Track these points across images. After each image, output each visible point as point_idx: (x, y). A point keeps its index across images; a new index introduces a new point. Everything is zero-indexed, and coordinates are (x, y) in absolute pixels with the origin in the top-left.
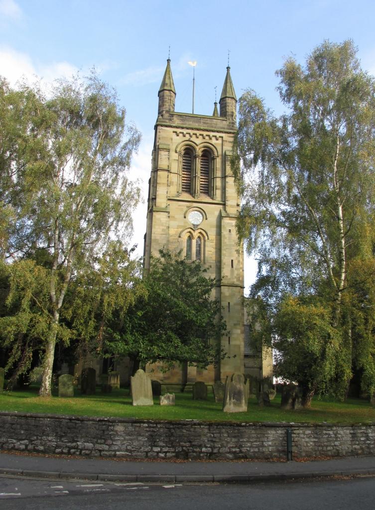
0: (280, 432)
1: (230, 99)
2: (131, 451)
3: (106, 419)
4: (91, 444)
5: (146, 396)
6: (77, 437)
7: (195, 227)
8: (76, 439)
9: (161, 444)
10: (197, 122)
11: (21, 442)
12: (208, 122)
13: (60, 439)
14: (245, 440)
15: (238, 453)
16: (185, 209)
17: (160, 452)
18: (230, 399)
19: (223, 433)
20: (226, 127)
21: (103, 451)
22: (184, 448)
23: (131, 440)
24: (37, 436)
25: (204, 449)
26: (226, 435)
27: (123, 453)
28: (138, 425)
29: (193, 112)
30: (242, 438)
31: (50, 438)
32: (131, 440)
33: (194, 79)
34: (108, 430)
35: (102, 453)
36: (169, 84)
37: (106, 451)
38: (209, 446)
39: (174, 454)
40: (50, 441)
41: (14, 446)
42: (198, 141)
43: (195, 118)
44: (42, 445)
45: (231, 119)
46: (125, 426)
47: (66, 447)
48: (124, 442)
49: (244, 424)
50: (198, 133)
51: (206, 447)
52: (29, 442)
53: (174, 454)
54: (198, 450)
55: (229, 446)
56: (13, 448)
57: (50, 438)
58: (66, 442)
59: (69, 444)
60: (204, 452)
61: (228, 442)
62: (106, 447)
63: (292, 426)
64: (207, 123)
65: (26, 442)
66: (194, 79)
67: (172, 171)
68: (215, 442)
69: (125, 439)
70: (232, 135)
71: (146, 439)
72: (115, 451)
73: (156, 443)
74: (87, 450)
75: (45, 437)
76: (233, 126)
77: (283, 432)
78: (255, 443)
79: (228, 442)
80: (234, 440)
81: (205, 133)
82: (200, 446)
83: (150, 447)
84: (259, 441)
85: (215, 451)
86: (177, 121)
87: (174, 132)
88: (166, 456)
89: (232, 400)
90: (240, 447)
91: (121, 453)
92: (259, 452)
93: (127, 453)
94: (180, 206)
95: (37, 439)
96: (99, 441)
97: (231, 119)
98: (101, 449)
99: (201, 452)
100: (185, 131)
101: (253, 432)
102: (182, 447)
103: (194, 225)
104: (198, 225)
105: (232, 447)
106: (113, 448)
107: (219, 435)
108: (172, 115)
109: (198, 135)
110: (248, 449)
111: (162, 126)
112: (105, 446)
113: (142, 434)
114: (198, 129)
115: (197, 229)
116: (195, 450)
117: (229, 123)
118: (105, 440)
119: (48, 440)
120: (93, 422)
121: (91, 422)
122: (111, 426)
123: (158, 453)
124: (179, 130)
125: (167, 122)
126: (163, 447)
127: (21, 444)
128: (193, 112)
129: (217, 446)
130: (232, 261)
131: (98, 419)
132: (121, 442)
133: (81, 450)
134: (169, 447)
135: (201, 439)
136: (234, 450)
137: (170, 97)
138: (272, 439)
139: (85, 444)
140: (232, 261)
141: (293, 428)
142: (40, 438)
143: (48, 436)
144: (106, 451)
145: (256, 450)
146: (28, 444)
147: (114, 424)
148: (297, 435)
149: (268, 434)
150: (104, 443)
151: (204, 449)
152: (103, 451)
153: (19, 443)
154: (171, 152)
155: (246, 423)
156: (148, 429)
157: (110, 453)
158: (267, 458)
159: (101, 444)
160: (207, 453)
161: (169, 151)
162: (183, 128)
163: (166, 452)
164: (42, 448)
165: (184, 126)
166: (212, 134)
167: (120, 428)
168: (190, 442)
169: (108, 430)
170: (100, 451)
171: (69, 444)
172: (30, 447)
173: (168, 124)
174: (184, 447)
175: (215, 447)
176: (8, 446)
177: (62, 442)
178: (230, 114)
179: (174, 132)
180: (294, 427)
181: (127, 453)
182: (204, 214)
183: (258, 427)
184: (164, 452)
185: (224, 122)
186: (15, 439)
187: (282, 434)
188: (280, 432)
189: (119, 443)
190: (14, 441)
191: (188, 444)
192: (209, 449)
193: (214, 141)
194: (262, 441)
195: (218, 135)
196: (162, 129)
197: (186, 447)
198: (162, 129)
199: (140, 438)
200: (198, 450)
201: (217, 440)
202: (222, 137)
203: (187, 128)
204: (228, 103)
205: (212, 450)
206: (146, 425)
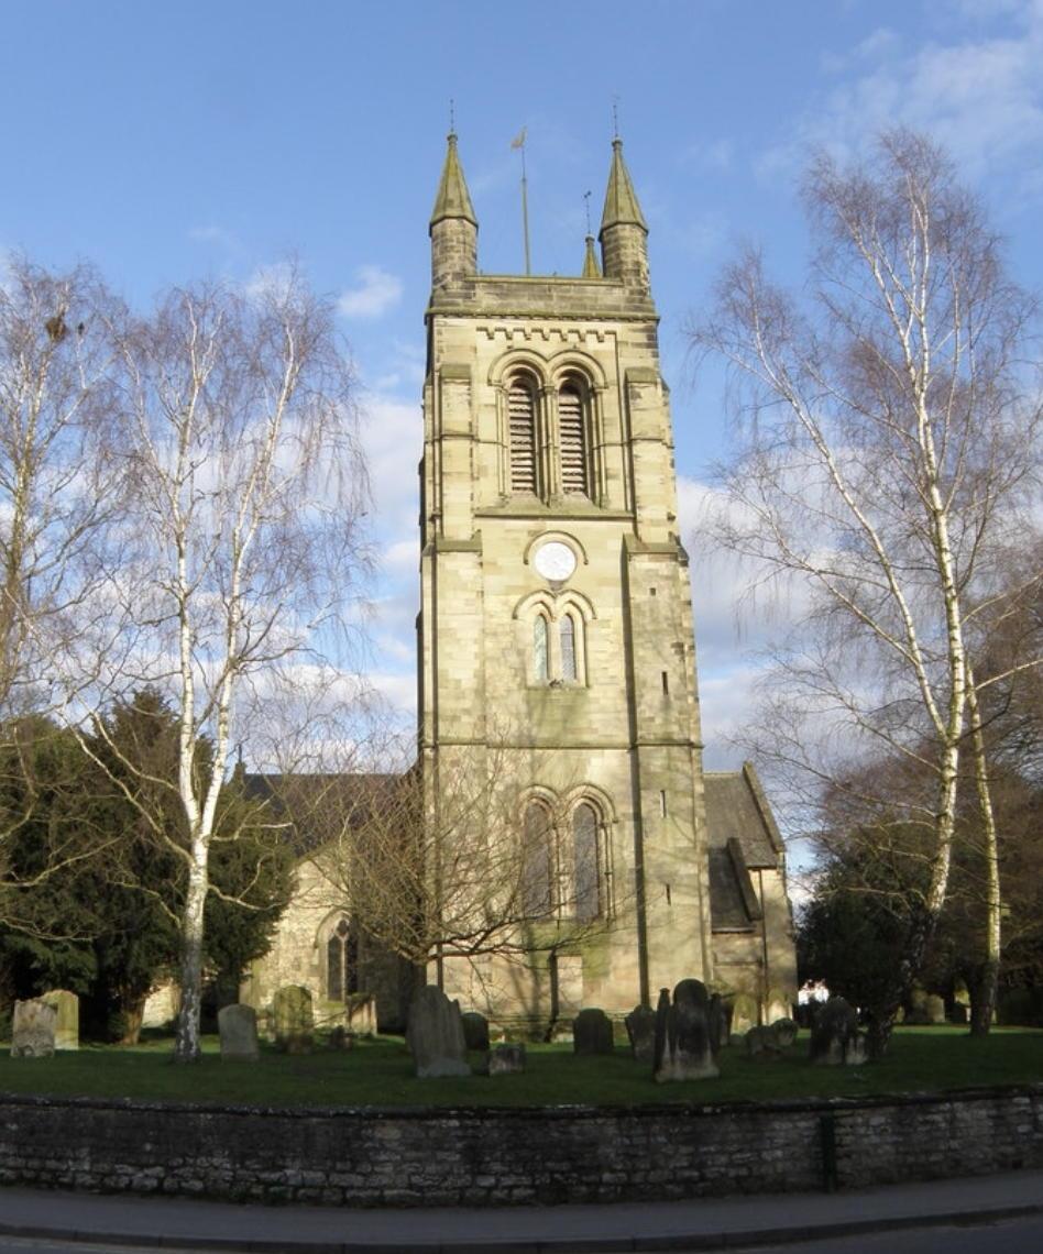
0: (802, 1124)
1: (628, 227)
2: (420, 1189)
3: (352, 1112)
4: (320, 1174)
5: (450, 1053)
6: (283, 1158)
7: (556, 588)
8: (281, 1163)
9: (497, 1167)
10: (541, 298)
11: (147, 1171)
12: (572, 294)
13: (242, 1164)
14: (712, 1149)
15: (696, 1183)
16: (525, 539)
17: (495, 1187)
18: (672, 1050)
19: (655, 1135)
20: (623, 304)
21: (352, 1188)
22: (557, 1176)
23: (419, 1160)
24: (184, 1156)
25: (607, 1176)
26: (662, 1139)
27: (402, 1191)
28: (434, 1122)
29: (528, 272)
30: (706, 1144)
31: (216, 1161)
32: (419, 1160)
33: (524, 180)
34: (358, 1137)
35: (350, 1194)
36: (456, 203)
37: (359, 1188)
38: (619, 1167)
39: (530, 1192)
40: (216, 1168)
41: (131, 1182)
42: (547, 349)
43: (536, 288)
44: (201, 1179)
45: (634, 283)
46: (400, 1128)
47: (259, 1181)
48: (404, 1166)
49: (707, 1110)
50: (546, 325)
51: (613, 1171)
52: (166, 1171)
53: (530, 1192)
54: (593, 1178)
55: (671, 1166)
56: (129, 1188)
57: (216, 1161)
58: (254, 1170)
59: (264, 1176)
60: (608, 1184)
61: (668, 1157)
62: (358, 1180)
63: (833, 1107)
64: (571, 298)
65: (159, 1170)
66: (524, 180)
67: (481, 437)
68: (635, 1156)
69: (404, 1161)
70: (641, 325)
71: (458, 1157)
72: (382, 1188)
73: (483, 1167)
74: (311, 1187)
75: (203, 1159)
76: (641, 301)
77: (811, 1124)
78: (738, 1156)
79: (668, 1157)
80: (684, 1150)
81: (566, 326)
82: (599, 1169)
83: (468, 1177)
84: (751, 1151)
85: (638, 1178)
86: (485, 299)
87: (480, 329)
88: (510, 1195)
89: (679, 1052)
90: (701, 1166)
91: (395, 1192)
92: (750, 1176)
93: (413, 1193)
94: (508, 531)
95: (184, 1165)
96: (339, 1166)
97: (634, 283)
98: (343, 1184)
99: (600, 1183)
100: (510, 324)
101: (731, 1128)
102: (552, 1172)
103: (550, 581)
104: (562, 583)
105: (682, 1168)
106: (375, 1181)
107: (643, 1140)
108: (471, 285)
109: (546, 331)
110: (723, 1170)
111: (445, 315)
112: (353, 1176)
113: (446, 1146)
114: (546, 317)
115: (563, 593)
116: (584, 1178)
117: (632, 292)
118: (355, 1162)
119: (212, 1165)
120: (320, 1120)
121: (315, 1120)
122: (366, 1127)
123: (490, 1189)
124: (493, 324)
125: (458, 305)
126: (503, 1174)
127: (147, 1176)
128: (528, 272)
129: (643, 1166)
130: (664, 674)
131: (331, 1113)
132: (395, 1168)
133: (297, 1188)
134: (517, 1174)
135: (600, 1152)
136: (687, 1174)
137: (461, 237)
138: (781, 1141)
139: (305, 1174)
140: (664, 674)
141: (837, 1113)
142: (191, 1161)
143: (212, 1156)
144: (359, 1188)
145: (744, 1172)
146: (162, 1175)
147: (372, 1122)
148: (849, 1130)
149: (774, 1130)
150: (352, 1171)
151: (607, 1176)
152: (352, 1188)
153: (140, 1175)
154: (475, 385)
155: (715, 1105)
156: (460, 1133)
157: (369, 1192)
158: (779, 1188)
159: (343, 1172)
160: (616, 1185)
161: (469, 383)
162: (503, 316)
163: (511, 1188)
164: (198, 1185)
165: (508, 311)
166: (584, 326)
167: (390, 1133)
168: (570, 1159)
169: (358, 1137)
170: (344, 1189)
171: (264, 1176)
172: (168, 1183)
173: (461, 308)
174: (557, 1172)
175: (635, 1171)
176: (116, 1183)
177: (247, 1169)
178: (630, 267)
179: (480, 329)
180: (840, 1108)
181: (413, 1193)
182: (550, 536)
183: (745, 1115)
184: (504, 1188)
185: (617, 291)
186: (130, 1164)
187: (807, 1129)
188: (805, 1125)
189: (389, 1169)
190: (130, 1170)
191: (565, 1166)
192: (620, 1175)
193: (592, 345)
194: (757, 1150)
195: (602, 327)
196: (446, 325)
197: (562, 1173)
198: (446, 325)
199: (441, 1155)
200: (593, 1178)
201: (641, 1153)
202: (614, 333)
203: (516, 316)
204: (624, 238)
205: (629, 1176)
206: (455, 1123)
